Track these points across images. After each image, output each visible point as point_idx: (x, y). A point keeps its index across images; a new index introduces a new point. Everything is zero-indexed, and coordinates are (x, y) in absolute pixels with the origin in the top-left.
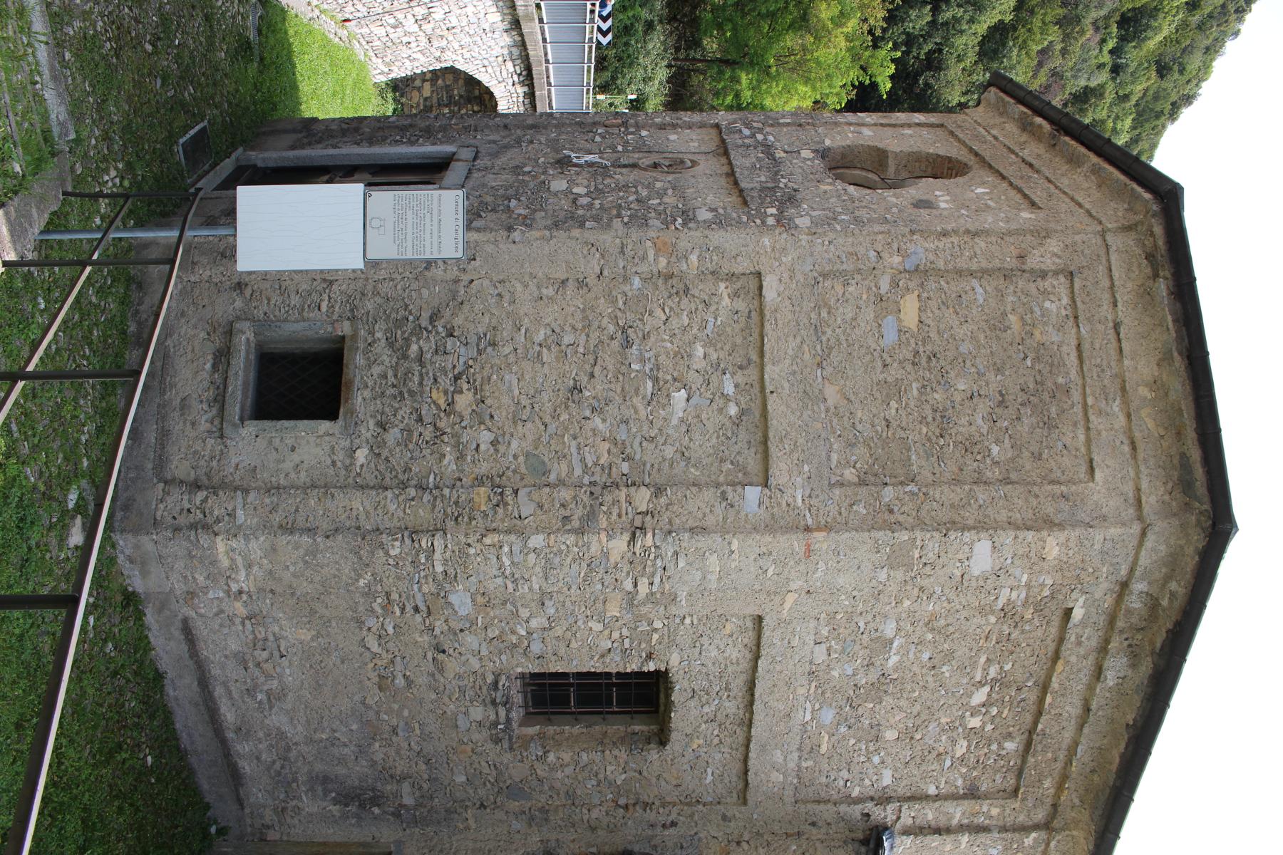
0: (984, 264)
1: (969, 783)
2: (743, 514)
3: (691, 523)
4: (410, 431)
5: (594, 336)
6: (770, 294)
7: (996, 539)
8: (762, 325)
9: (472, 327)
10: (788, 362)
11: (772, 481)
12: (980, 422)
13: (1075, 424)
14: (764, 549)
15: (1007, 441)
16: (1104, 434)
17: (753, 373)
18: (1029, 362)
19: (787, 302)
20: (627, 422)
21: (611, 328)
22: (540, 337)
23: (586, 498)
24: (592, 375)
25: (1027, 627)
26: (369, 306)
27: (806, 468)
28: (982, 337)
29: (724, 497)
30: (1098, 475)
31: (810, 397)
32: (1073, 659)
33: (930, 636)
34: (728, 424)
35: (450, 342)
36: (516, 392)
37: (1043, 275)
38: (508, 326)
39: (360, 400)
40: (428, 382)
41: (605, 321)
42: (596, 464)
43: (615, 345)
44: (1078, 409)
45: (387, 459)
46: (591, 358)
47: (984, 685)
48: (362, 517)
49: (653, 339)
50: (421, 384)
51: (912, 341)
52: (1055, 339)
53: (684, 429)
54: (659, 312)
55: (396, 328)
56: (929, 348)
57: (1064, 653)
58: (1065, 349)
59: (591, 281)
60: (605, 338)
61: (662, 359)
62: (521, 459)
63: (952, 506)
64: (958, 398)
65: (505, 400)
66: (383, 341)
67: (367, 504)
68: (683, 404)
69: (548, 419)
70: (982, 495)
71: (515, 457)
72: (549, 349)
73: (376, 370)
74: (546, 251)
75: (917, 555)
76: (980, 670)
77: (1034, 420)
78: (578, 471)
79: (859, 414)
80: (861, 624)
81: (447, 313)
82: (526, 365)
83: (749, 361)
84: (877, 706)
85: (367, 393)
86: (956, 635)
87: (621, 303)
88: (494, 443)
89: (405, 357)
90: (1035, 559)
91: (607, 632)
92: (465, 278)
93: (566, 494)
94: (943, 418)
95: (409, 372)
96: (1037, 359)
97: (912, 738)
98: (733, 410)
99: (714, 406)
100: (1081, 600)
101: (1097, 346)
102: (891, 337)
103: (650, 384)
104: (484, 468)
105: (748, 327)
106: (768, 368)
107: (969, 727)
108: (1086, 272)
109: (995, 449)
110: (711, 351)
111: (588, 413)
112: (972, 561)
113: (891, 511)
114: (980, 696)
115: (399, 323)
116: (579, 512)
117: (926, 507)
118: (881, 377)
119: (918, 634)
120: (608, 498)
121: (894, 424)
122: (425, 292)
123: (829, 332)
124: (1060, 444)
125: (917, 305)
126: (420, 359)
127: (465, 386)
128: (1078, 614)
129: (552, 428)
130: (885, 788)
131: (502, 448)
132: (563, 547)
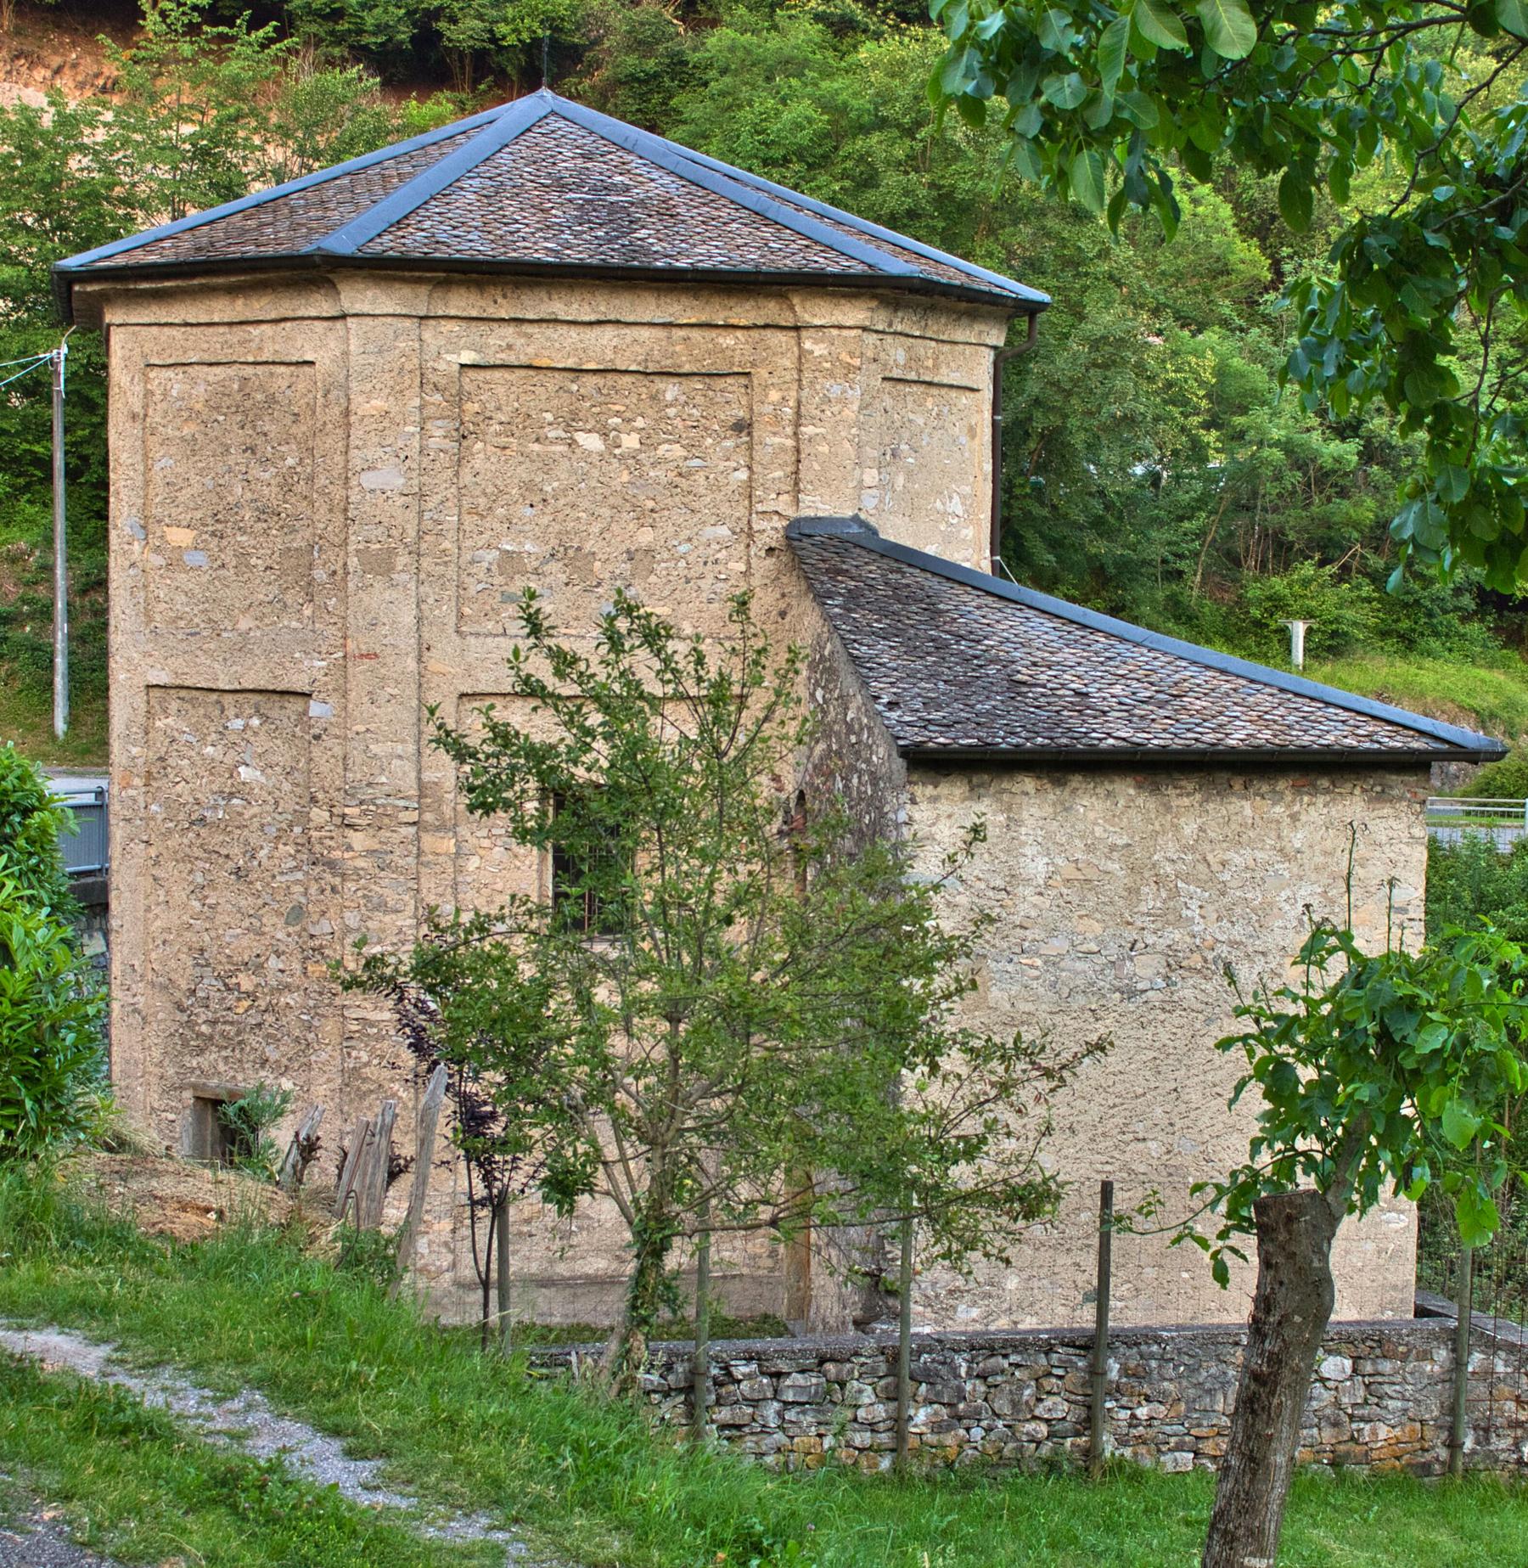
0: (139, 458)
1: (730, 432)
2: (333, 720)
3: (340, 770)
4: (269, 1036)
5: (198, 853)
6: (163, 678)
7: (358, 469)
8: (188, 688)
9: (188, 971)
10: (216, 665)
11: (306, 689)
12: (267, 475)
13: (272, 374)
14: (365, 699)
15: (283, 449)
16: (277, 347)
17: (228, 699)
18: (221, 418)
19: (169, 661)
20: (262, 825)
21: (191, 835)
22: (197, 904)
23: (318, 869)
24: (227, 856)
25: (491, 406)
26: (171, 1071)
27: (297, 655)
28: (200, 465)
29: (317, 737)
30: (308, 358)
31: (243, 646)
32: (530, 350)
33: (500, 511)
34: (265, 728)
35: (200, 994)
36: (239, 931)
37: (148, 394)
38: (188, 936)
39: (246, 1080)
40: (231, 1016)
41: (186, 841)
42: (295, 858)
43: (204, 832)
44: (260, 369)
45: (290, 1059)
46: (215, 856)
47: (575, 441)
48: (331, 1085)
49: (199, 796)
50: (232, 1023)
51: (205, 537)
52: (202, 389)
53: (269, 771)
54: (179, 788)
55: (188, 1045)
56: (210, 521)
57: (524, 360)
58: (211, 379)
59: (153, 852)
60: (200, 841)
61: (215, 788)
62: (291, 929)
63: (331, 511)
64: (249, 495)
65: (245, 942)
66: (200, 1059)
67: (321, 1081)
68: (249, 770)
69: (260, 902)
70: (322, 481)
71: (289, 935)
72: (206, 897)
73: (222, 1067)
74: (127, 894)
75: (378, 546)
76: (553, 448)
77: (267, 418)
78: (299, 875)
79: (261, 596)
80: (480, 587)
81: (178, 994)
82: (219, 919)
83: (218, 702)
84: (600, 556)
85: (240, 1077)
86: (498, 483)
87: (171, 825)
88: (278, 954)
89: (211, 1038)
90: (386, 423)
91: (482, 852)
92: (150, 976)
93: (313, 890)
94: (265, 513)
95: (222, 1034)
96: (217, 408)
97: (652, 511)
98: (255, 722)
99: (252, 739)
100: (449, 357)
101: (205, 346)
102: (200, 558)
103: (235, 801)
104: (297, 966)
105: (191, 701)
106: (222, 686)
107: (638, 446)
108: (146, 350)
109: (290, 461)
110: (209, 739)
111: (256, 863)
112: (386, 488)
113: (335, 572)
114: (591, 442)
115: (185, 1044)
116: (328, 876)
117: (332, 538)
118: (232, 571)
119: (496, 525)
120: (317, 848)
121: (269, 562)
122: (161, 1016)
123: (196, 620)
124: (288, 392)
125: (175, 529)
126: (213, 1023)
127: (234, 980)
128: (468, 357)
129: (268, 899)
130: (734, 533)
131: (282, 948)
132: (360, 893)
